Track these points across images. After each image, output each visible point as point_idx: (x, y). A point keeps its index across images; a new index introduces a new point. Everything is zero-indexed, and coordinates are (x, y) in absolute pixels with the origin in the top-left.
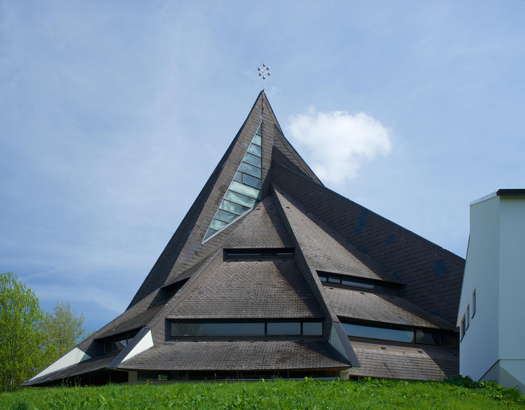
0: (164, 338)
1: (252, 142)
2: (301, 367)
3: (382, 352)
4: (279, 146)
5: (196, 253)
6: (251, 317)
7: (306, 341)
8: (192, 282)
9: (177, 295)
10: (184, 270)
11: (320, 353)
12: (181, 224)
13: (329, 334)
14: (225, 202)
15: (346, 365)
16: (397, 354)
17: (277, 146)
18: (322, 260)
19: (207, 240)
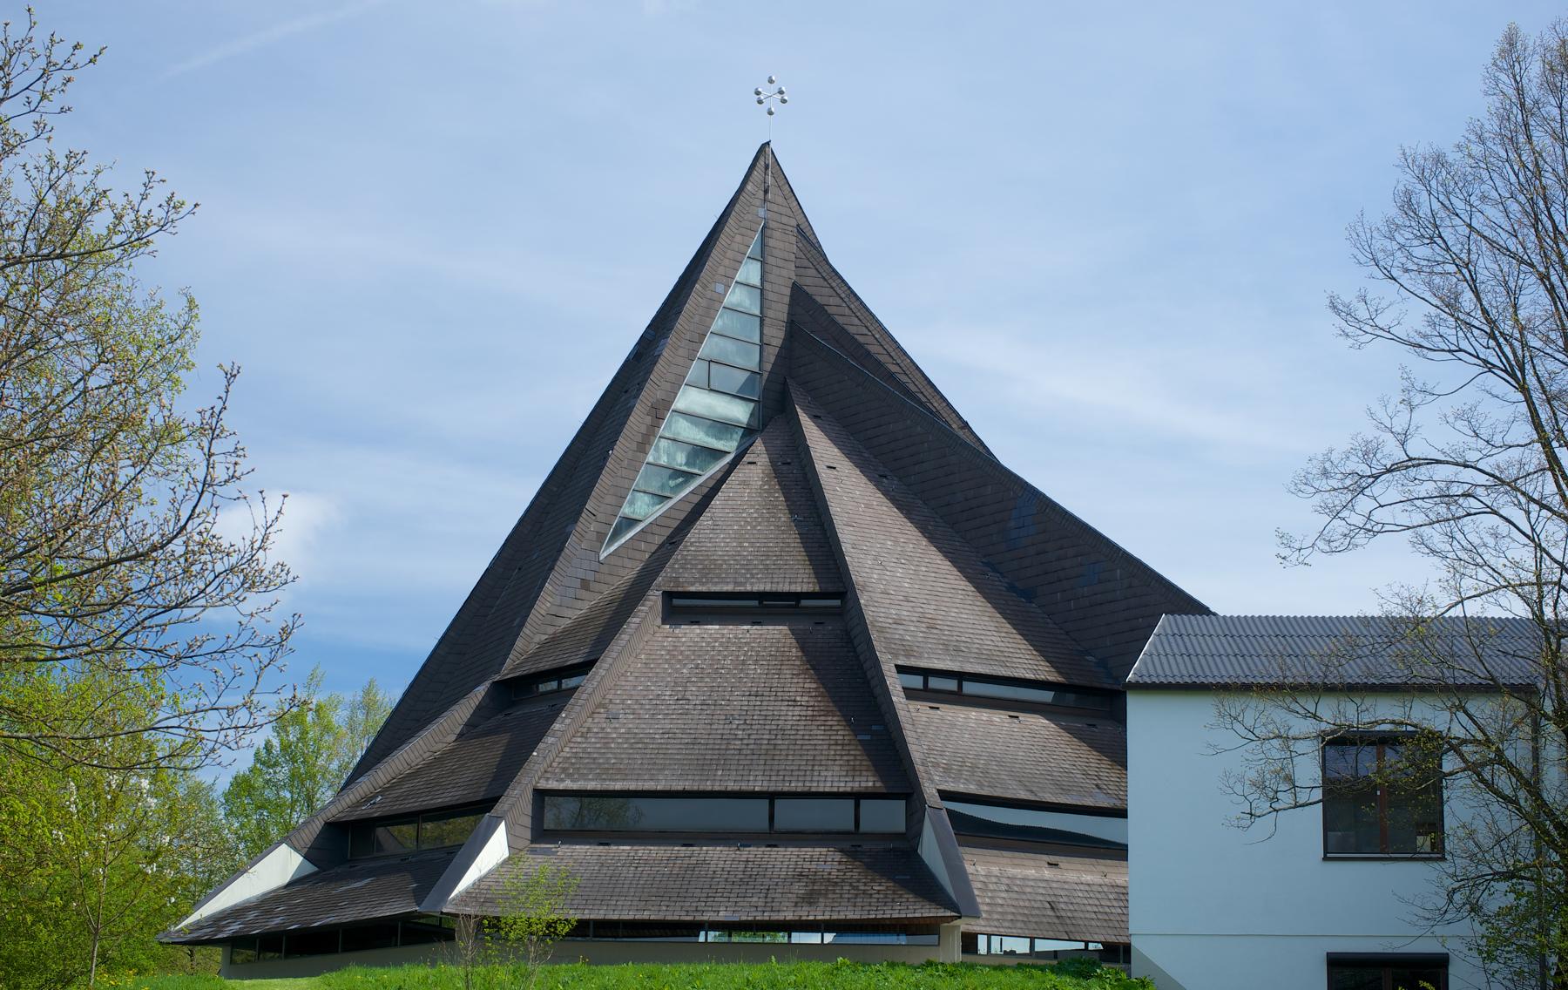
0: (528, 835)
1: (737, 278)
2: (851, 916)
3: (1048, 873)
4: (811, 283)
5: (585, 585)
6: (737, 788)
7: (866, 847)
8: (589, 690)
9: (556, 726)
10: (551, 630)
11: (894, 881)
12: (539, 494)
13: (919, 834)
14: (664, 443)
15: (949, 914)
16: (1088, 878)
17: (801, 281)
18: (912, 633)
19: (612, 549)
